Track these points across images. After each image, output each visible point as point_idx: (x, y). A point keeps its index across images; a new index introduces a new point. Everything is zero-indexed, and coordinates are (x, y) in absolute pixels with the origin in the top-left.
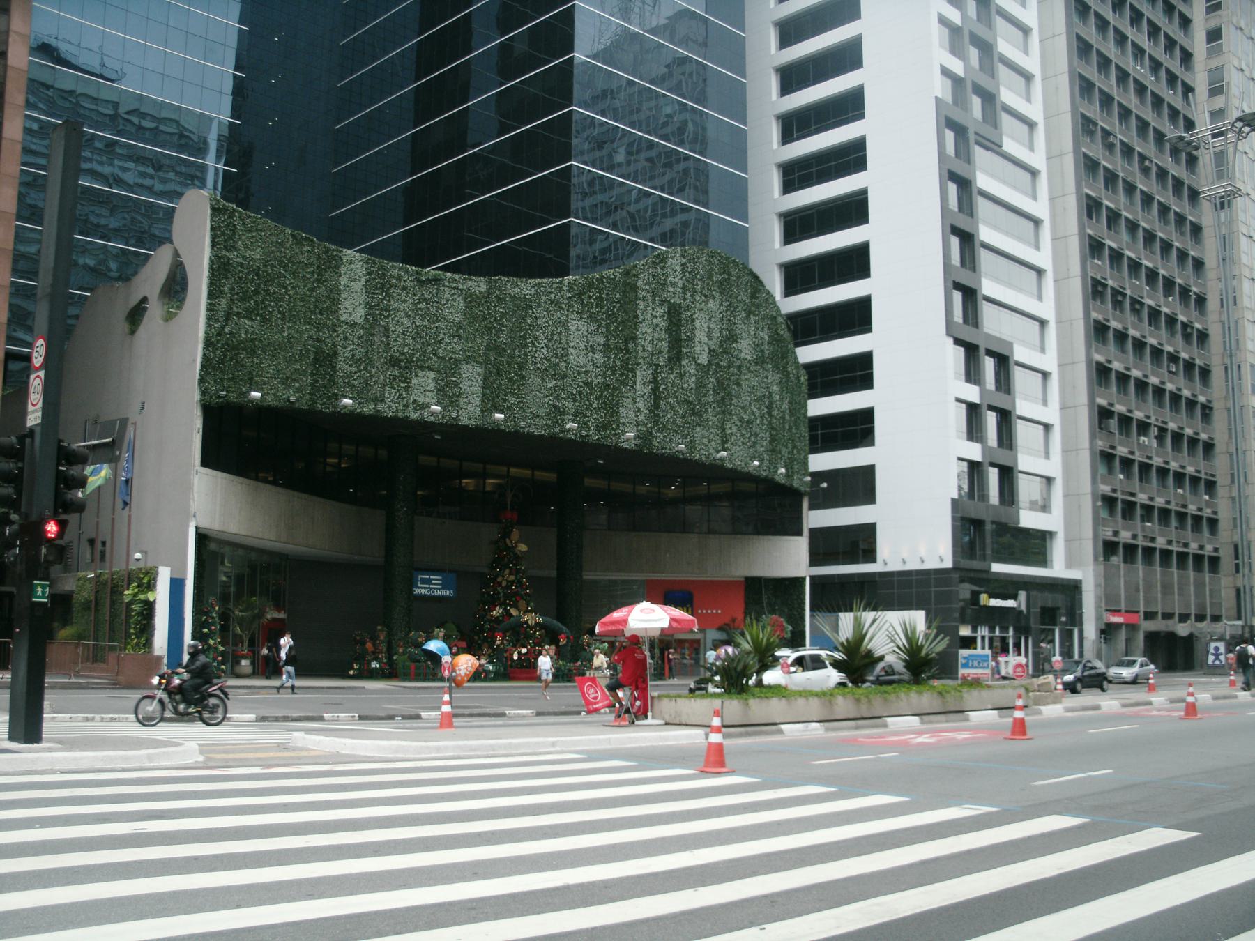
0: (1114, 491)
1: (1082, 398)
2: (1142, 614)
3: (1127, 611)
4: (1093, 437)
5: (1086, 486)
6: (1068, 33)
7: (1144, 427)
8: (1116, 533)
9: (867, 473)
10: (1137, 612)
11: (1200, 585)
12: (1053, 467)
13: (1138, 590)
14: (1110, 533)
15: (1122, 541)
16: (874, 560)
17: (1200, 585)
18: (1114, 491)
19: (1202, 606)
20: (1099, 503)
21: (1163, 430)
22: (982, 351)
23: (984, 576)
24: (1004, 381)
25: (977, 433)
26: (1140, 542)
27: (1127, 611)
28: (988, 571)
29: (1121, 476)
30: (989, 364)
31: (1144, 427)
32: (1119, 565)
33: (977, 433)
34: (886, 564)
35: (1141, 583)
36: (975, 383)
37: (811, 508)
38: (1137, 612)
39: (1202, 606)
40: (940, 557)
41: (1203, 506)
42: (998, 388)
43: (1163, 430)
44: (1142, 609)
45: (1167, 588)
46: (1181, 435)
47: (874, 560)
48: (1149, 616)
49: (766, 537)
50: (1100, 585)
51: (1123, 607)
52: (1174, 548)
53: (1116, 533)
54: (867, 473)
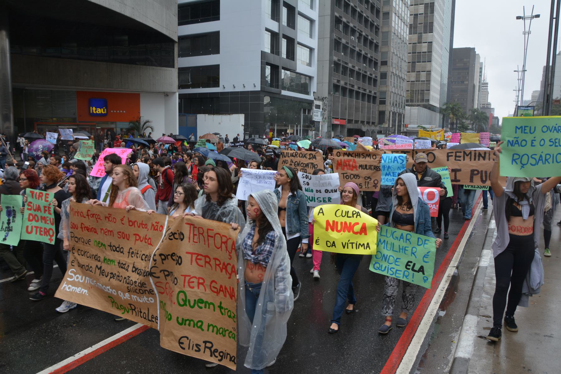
0: (339, 60)
1: (328, 11)
2: (347, 120)
3: (341, 119)
4: (332, 32)
5: (327, 57)
6: (330, 38)
7: (353, 31)
8: (338, 81)
9: (216, 35)
10: (345, 119)
11: (369, 108)
12: (314, 43)
13: (346, 109)
14: (336, 81)
15: (341, 85)
16: (218, 86)
17: (369, 108)
18: (339, 60)
19: (369, 118)
20: (333, 65)
21: (360, 35)
22: (280, 68)
23: (277, 96)
24: (292, 23)
25: (277, 17)
26: (348, 87)
27: (341, 119)
28: (279, 94)
29: (343, 54)
30: (284, 11)
31: (353, 31)
32: (339, 97)
33: (277, 17)
34: (224, 88)
35: (347, 106)
36: (276, 21)
37: (180, 55)
38: (345, 119)
39: (369, 118)
40: (254, 84)
41: (372, 73)
42: (288, 57)
43: (360, 35)
44: (347, 118)
45: (357, 109)
46: (366, 57)
47: (218, 86)
48: (350, 121)
49: (151, 67)
50: (330, 127)
51: (340, 117)
52: (361, 91)
53: (338, 81)
54: (216, 35)
